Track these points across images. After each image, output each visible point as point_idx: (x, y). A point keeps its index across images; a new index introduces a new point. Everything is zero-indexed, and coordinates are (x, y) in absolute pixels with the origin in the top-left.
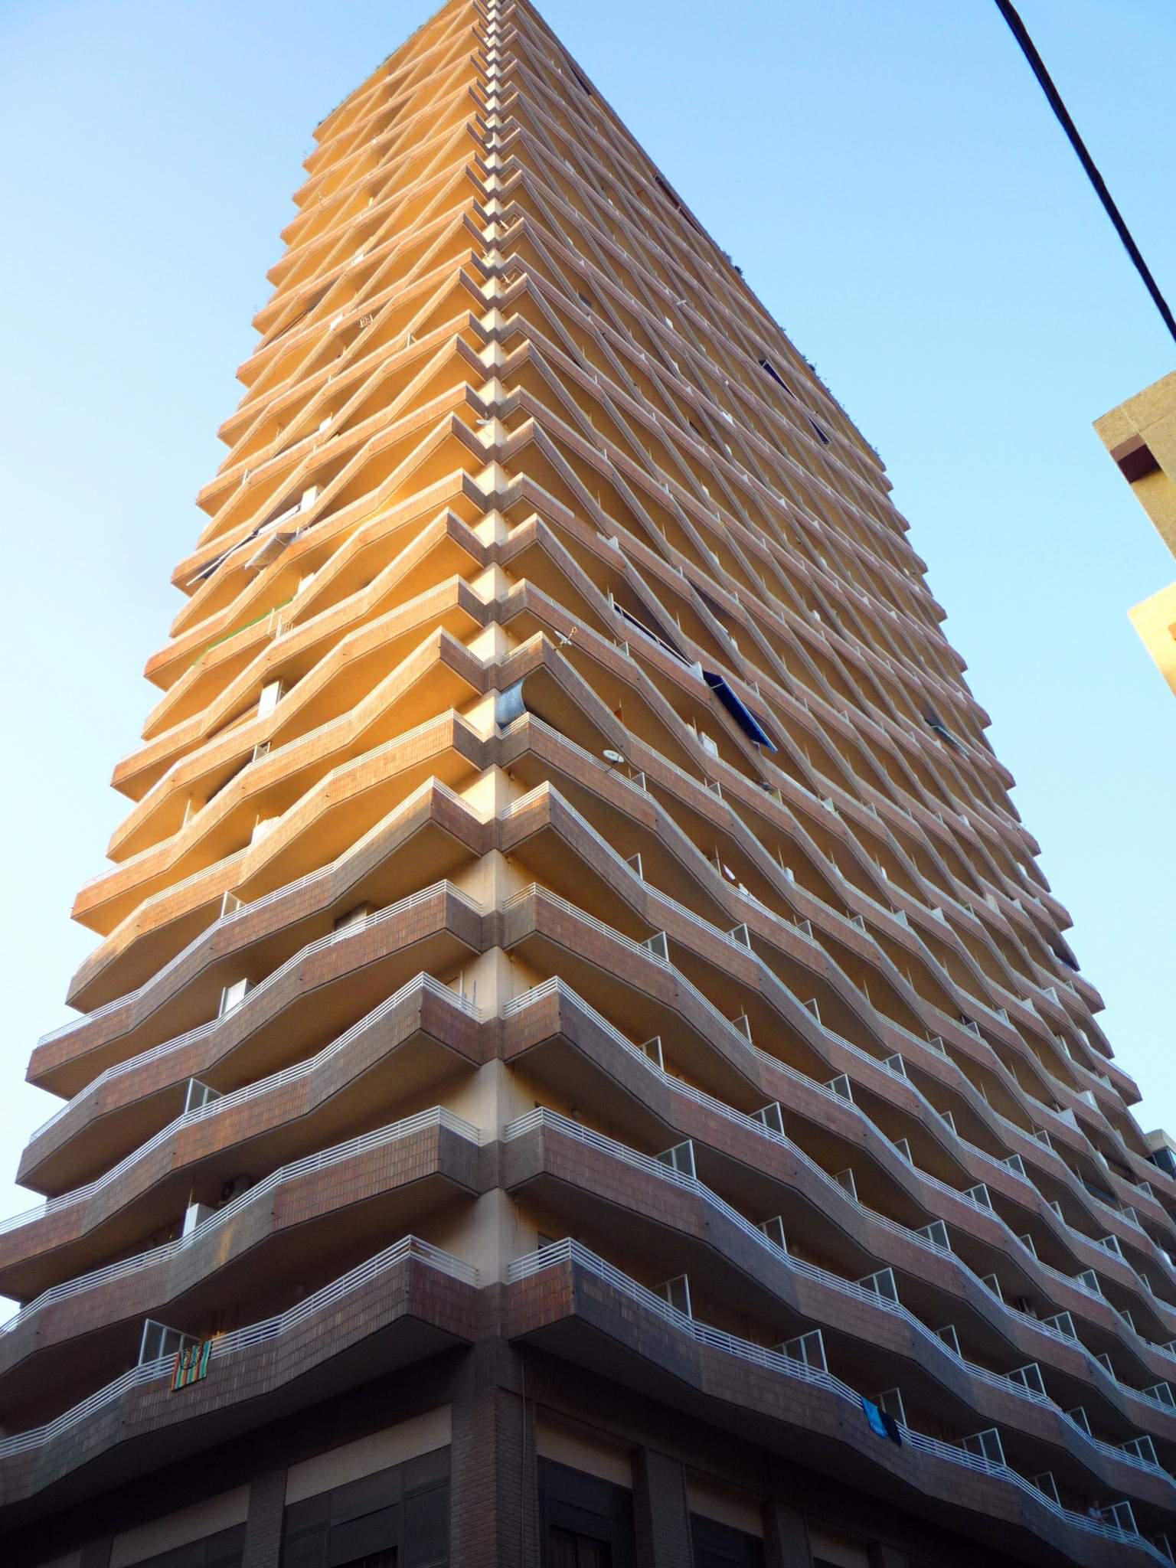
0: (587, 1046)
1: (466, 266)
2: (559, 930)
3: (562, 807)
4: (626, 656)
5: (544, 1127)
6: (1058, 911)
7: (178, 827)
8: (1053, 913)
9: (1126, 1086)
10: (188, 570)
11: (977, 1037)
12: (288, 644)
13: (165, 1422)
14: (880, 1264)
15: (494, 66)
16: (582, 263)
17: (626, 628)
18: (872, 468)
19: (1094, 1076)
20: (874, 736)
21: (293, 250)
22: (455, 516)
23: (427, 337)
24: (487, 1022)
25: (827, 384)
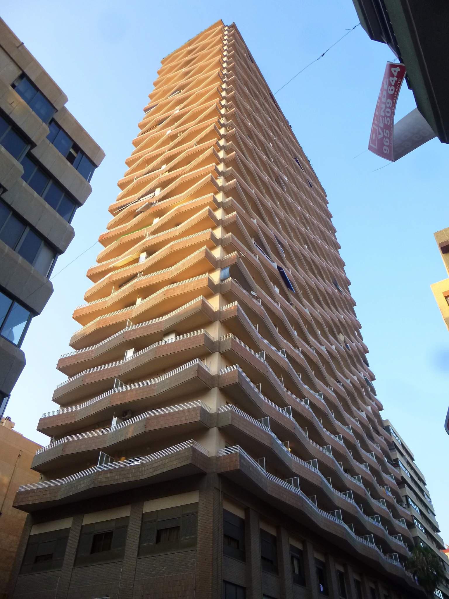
0: (244, 387)
1: (216, 123)
2: (237, 349)
3: (240, 310)
4: (257, 260)
5: (231, 410)
6: (365, 348)
7: (109, 294)
8: (364, 348)
9: (380, 406)
10: (114, 207)
11: (342, 387)
12: (151, 241)
13: (107, 484)
14: (313, 458)
15: (226, 52)
16: (249, 124)
17: (257, 250)
18: (322, 195)
19: (371, 401)
20: (320, 287)
21: (152, 102)
22: (210, 209)
23: (201, 145)
24: (214, 375)
25: (313, 167)
